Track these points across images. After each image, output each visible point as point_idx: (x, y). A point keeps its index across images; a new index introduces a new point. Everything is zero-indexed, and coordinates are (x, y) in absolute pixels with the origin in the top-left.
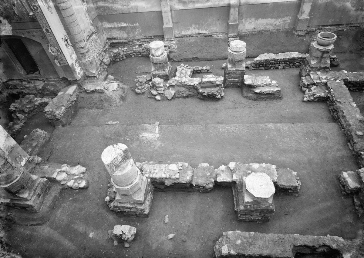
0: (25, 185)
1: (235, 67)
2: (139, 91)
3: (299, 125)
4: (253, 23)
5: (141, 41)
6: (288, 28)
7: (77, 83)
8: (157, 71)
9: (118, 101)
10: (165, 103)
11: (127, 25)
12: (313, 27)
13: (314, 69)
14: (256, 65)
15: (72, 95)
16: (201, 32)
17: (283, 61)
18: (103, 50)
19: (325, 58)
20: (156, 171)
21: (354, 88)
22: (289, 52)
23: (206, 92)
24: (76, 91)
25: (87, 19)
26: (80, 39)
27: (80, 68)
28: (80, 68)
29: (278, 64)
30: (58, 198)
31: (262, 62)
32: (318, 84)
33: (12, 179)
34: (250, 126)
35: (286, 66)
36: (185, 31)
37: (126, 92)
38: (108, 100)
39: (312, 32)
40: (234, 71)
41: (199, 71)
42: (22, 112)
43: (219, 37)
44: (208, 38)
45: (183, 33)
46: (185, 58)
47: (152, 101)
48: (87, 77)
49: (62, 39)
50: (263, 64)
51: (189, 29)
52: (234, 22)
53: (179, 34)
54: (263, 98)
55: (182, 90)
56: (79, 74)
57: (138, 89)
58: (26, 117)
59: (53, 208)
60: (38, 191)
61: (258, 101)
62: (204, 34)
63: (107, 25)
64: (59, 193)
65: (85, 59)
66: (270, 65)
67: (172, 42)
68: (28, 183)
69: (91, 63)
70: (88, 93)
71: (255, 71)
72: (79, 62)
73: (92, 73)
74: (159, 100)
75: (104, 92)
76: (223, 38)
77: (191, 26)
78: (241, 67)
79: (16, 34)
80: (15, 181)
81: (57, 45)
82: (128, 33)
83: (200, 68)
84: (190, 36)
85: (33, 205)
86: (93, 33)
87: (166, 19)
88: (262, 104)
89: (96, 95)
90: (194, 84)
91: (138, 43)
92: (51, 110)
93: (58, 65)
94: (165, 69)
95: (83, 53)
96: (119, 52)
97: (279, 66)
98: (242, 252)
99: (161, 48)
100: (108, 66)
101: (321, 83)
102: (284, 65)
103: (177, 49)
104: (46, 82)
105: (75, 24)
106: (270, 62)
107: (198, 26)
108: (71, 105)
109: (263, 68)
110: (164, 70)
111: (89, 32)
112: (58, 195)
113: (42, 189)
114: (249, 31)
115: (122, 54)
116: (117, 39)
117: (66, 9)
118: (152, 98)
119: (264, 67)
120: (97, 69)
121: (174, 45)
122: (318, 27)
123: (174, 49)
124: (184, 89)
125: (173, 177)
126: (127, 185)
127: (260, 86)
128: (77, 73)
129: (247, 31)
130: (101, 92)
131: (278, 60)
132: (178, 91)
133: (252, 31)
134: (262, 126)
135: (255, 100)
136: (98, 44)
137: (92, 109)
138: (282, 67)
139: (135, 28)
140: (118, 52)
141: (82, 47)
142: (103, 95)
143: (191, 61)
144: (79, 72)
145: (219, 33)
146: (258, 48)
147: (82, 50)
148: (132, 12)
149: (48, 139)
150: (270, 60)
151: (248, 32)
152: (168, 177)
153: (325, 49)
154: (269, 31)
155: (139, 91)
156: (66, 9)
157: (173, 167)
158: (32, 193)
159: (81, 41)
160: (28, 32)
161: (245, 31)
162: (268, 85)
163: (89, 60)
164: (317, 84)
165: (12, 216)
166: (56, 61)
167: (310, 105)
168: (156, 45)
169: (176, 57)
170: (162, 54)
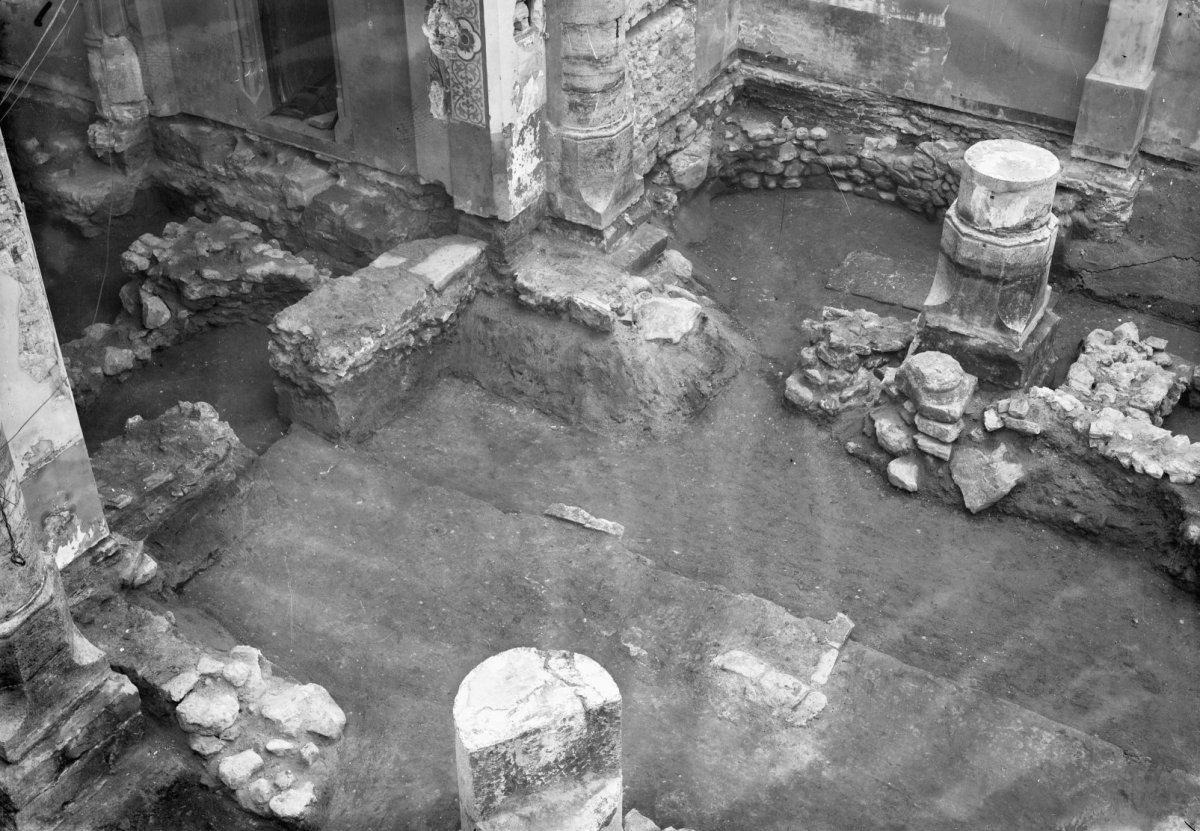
2: (807, 394)
7: (486, 237)
8: (955, 318)
9: (666, 405)
15: (439, 292)
27: (536, 161)
28: (536, 161)
37: (728, 372)
38: (614, 382)
42: (171, 289)
46: (1161, 292)
56: (519, 192)
73: (585, 208)
74: (904, 492)
87: (1123, 35)
92: (307, 331)
94: (1012, 319)
96: (775, 140)
99: (1034, 192)
103: (1127, 228)
104: (342, 182)
110: (1000, 326)
116: (792, 70)
118: (868, 462)
121: (1119, 200)
128: (513, 184)
130: (599, 328)
136: (680, 66)
141: (589, 59)
142: (595, 347)
144: (526, 180)
147: (585, 69)
155: (807, 394)
170: (1027, 227)
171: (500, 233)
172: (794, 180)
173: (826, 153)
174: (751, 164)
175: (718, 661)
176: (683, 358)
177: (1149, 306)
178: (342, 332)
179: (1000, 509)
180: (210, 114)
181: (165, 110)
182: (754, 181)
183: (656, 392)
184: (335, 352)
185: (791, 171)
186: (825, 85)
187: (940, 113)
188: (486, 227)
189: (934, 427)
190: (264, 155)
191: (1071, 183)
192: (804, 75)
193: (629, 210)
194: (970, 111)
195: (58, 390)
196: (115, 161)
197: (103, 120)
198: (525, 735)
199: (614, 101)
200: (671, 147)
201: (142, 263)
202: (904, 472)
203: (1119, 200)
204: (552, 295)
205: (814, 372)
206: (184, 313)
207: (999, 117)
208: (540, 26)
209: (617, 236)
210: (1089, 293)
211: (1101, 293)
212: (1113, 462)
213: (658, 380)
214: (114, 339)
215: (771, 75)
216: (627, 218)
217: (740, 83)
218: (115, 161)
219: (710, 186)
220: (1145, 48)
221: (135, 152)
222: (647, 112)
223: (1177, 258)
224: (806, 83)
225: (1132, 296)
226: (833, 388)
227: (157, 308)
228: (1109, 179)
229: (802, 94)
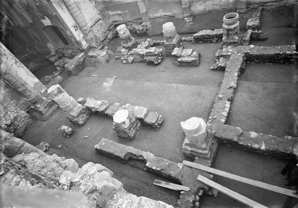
0: (38, 101)
1: (168, 42)
2: (117, 57)
3: (193, 86)
4: (202, 4)
5: (132, 22)
6: (232, 6)
7: (84, 51)
9: (104, 62)
10: (127, 65)
12: (255, 4)
13: (226, 44)
14: (196, 39)
15: (81, 58)
16: (167, 14)
17: (215, 36)
18: (108, 29)
19: (231, 34)
20: (91, 103)
21: (258, 61)
22: (217, 29)
23: (148, 59)
24: (84, 56)
25: (95, 11)
26: (83, 25)
27: (86, 42)
28: (86, 42)
29: (211, 38)
30: (55, 111)
31: (199, 37)
32: (225, 56)
33: (31, 97)
34: (162, 84)
35: (218, 40)
36: (156, 14)
37: (111, 57)
38: (98, 62)
39: (255, 9)
40: (168, 44)
41: (158, 44)
42: (59, 66)
43: (180, 17)
44: (172, 18)
45: (155, 15)
47: (121, 64)
48: (90, 48)
49: (72, 26)
50: (200, 39)
51: (158, 12)
52: (185, 5)
53: (153, 16)
54: (184, 65)
55: (137, 58)
56: (85, 46)
57: (117, 56)
58: (61, 69)
59: (52, 115)
60: (46, 105)
61: (181, 68)
62: (169, 15)
63: (111, 13)
64: (56, 108)
65: (88, 37)
66: (206, 39)
67: (147, 23)
68: (39, 100)
69: (92, 39)
70: (90, 57)
71: (195, 44)
72: (85, 39)
73: (93, 45)
75: (97, 57)
76: (181, 18)
77: (159, 10)
78: (172, 42)
79: (53, 25)
80: (32, 98)
81: (70, 30)
82: (123, 18)
83: (159, 41)
84: (160, 17)
85: (42, 111)
86: (99, 20)
88: (182, 69)
89: (93, 59)
90: (143, 54)
91: (130, 24)
92: (67, 66)
93: (73, 41)
94: (128, 43)
95: (86, 34)
97: (213, 41)
98: (102, 149)
99: (123, 29)
100: (110, 40)
101: (228, 56)
102: (217, 39)
103: (151, 27)
104: (73, 51)
105: (79, 17)
106: (205, 37)
107: (164, 10)
108: (79, 64)
109: (201, 42)
110: (127, 44)
111: (96, 19)
112: (55, 109)
113: (47, 105)
114: (201, 11)
116: (118, 22)
117: (72, 9)
119: (202, 41)
120: (96, 43)
121: (149, 25)
122: (259, 4)
123: (149, 27)
124: (138, 56)
125: (95, 107)
126: (63, 106)
127: (183, 56)
128: (84, 45)
129: (199, 11)
130: (96, 57)
131: (210, 35)
132: (135, 58)
133: (203, 11)
134: (169, 85)
135: (179, 66)
136: (103, 26)
137: (91, 67)
138: (216, 41)
139: (126, 14)
141: (85, 30)
142: (96, 59)
143: (160, 36)
144: (85, 44)
145: (179, 14)
146: (206, 25)
147: (85, 31)
148: (122, 3)
149: (61, 81)
150: (204, 36)
151: (200, 12)
152: (93, 107)
153: (228, 28)
154: (217, 10)
155: (117, 57)
156: (72, 9)
157: (99, 102)
158: (42, 105)
159: (84, 26)
160: (57, 24)
161: (198, 11)
162: (188, 56)
164: (224, 56)
165: (36, 115)
166: (72, 38)
167: (214, 73)
168: (120, 27)
169: (150, 33)
170: (124, 33)
171: (85, 51)
175: (103, 84)
176: (105, 57)
178: (70, 65)
179: (133, 62)
180: (60, 48)
181: (57, 49)
184: (70, 67)
188: (82, 51)
189: (124, 56)
190: (66, 50)
192: (119, 22)
193: (99, 44)
195: (34, 77)
196: (54, 56)
197: (52, 52)
198: (52, 91)
200: (107, 35)
201: (56, 65)
202: (124, 62)
203: (149, 25)
204: (91, 55)
205: (117, 54)
206: (61, 68)
208: (79, 28)
209: (97, 47)
212: (139, 54)
214: (56, 73)
215: (117, 23)
216: (98, 45)
217: (114, 25)
218: (54, 56)
221: (56, 54)
222: (101, 33)
225: (153, 35)
226: (119, 55)
227: (58, 68)
228: (147, 23)
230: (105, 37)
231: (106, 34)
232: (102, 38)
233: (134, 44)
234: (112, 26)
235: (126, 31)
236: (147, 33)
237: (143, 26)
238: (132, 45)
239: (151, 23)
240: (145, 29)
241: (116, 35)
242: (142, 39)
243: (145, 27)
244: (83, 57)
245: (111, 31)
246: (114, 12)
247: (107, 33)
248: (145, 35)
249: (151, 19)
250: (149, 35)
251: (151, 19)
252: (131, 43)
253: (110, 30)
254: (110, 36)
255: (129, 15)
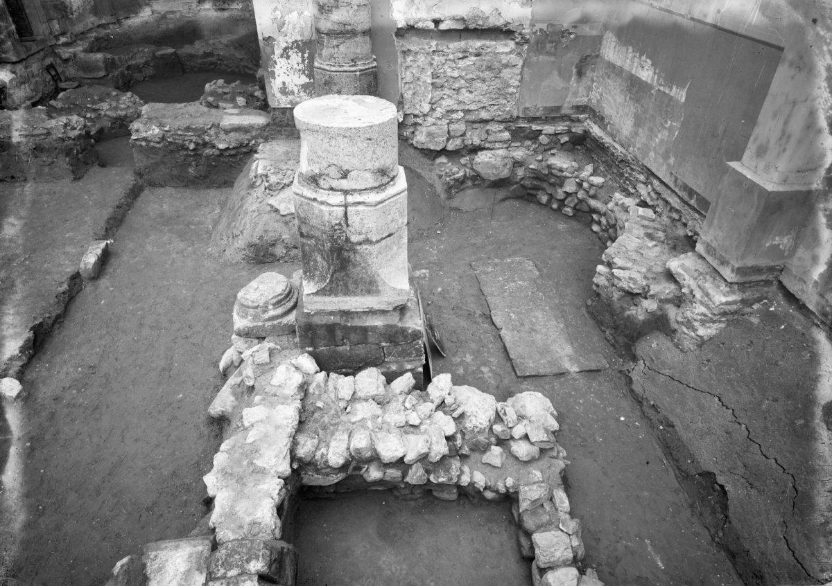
11: (653, 80)
46: (677, 423)
82: (638, 121)
96: (565, 174)
100: (476, 179)
103: (702, 343)
115: (570, 187)
116: (603, 127)
121: (702, 309)
136: (497, 84)
139: (666, 104)
140: (561, 170)
163: (327, 68)
169: (653, 371)
172: (569, 209)
173: (594, 197)
174: (545, 185)
177: (661, 427)
182: (544, 199)
183: (241, 232)
185: (570, 202)
186: (615, 144)
187: (663, 187)
191: (679, 274)
194: (677, 190)
199: (338, 46)
200: (477, 141)
203: (702, 309)
207: (692, 202)
210: (630, 381)
211: (637, 388)
213: (248, 226)
217: (578, 129)
219: (513, 188)
220: (789, 137)
223: (720, 400)
224: (607, 140)
229: (601, 147)
230: (458, 142)
231: (484, 136)
232: (430, 134)
233: (365, 330)
234: (561, 127)
235: (344, 184)
236: (641, 348)
237: (670, 276)
238: (337, 319)
239: (731, 317)
240: (650, 305)
241: (527, 183)
242: (572, 339)
243: (667, 289)
244: (248, 136)
245: (528, 143)
246: (624, 49)
247: (487, 132)
248: (622, 340)
249: (774, 288)
250: (637, 372)
251: (781, 286)
252: (327, 299)
253: (519, 135)
254: (490, 161)
255: (670, 129)
